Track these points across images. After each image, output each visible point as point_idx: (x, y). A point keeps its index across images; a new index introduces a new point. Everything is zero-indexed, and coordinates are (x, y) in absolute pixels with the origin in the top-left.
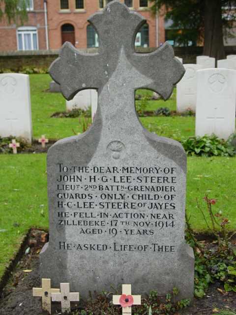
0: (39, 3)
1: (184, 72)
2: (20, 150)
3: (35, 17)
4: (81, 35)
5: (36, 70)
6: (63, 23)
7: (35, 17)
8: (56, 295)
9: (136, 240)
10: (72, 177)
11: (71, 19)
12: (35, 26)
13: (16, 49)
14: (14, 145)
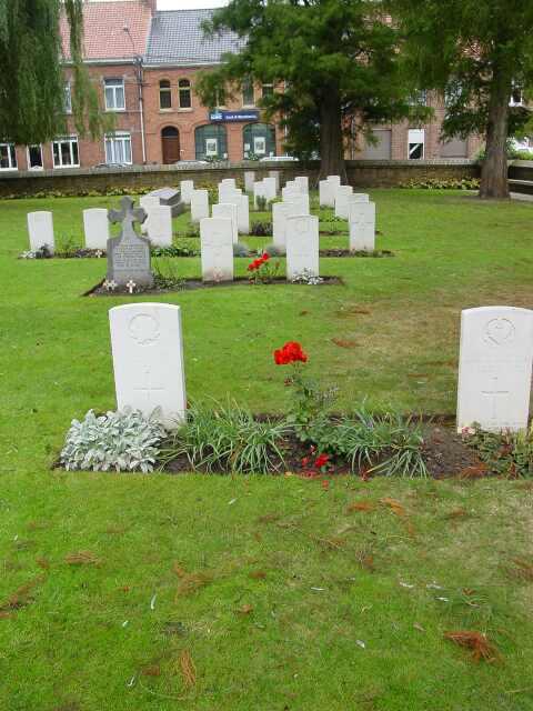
0: (133, 101)
1: (146, 217)
2: (102, 256)
3: (128, 119)
4: (187, 142)
5: (125, 190)
6: (163, 126)
7: (128, 119)
8: (110, 285)
9: (135, 268)
10: (65, 148)
11: (175, 121)
12: (128, 130)
13: (101, 393)
14: (99, 253)
